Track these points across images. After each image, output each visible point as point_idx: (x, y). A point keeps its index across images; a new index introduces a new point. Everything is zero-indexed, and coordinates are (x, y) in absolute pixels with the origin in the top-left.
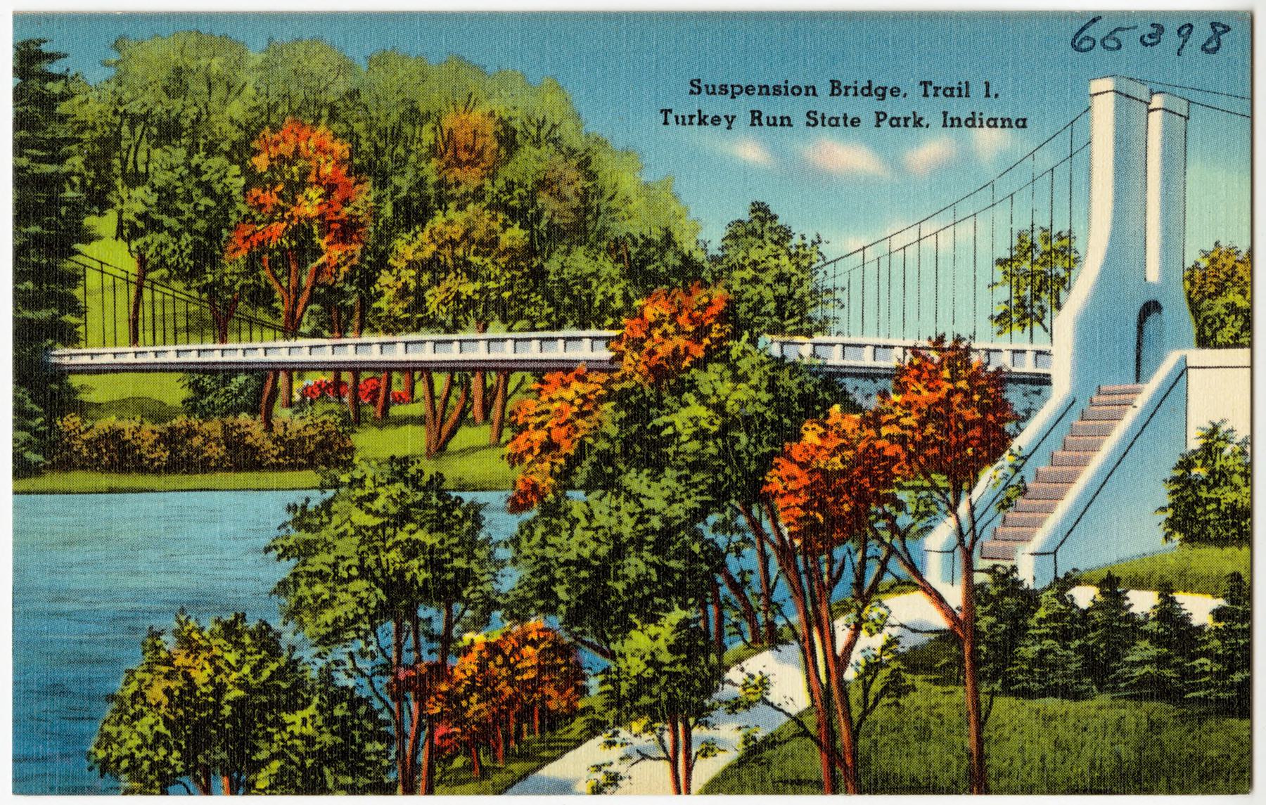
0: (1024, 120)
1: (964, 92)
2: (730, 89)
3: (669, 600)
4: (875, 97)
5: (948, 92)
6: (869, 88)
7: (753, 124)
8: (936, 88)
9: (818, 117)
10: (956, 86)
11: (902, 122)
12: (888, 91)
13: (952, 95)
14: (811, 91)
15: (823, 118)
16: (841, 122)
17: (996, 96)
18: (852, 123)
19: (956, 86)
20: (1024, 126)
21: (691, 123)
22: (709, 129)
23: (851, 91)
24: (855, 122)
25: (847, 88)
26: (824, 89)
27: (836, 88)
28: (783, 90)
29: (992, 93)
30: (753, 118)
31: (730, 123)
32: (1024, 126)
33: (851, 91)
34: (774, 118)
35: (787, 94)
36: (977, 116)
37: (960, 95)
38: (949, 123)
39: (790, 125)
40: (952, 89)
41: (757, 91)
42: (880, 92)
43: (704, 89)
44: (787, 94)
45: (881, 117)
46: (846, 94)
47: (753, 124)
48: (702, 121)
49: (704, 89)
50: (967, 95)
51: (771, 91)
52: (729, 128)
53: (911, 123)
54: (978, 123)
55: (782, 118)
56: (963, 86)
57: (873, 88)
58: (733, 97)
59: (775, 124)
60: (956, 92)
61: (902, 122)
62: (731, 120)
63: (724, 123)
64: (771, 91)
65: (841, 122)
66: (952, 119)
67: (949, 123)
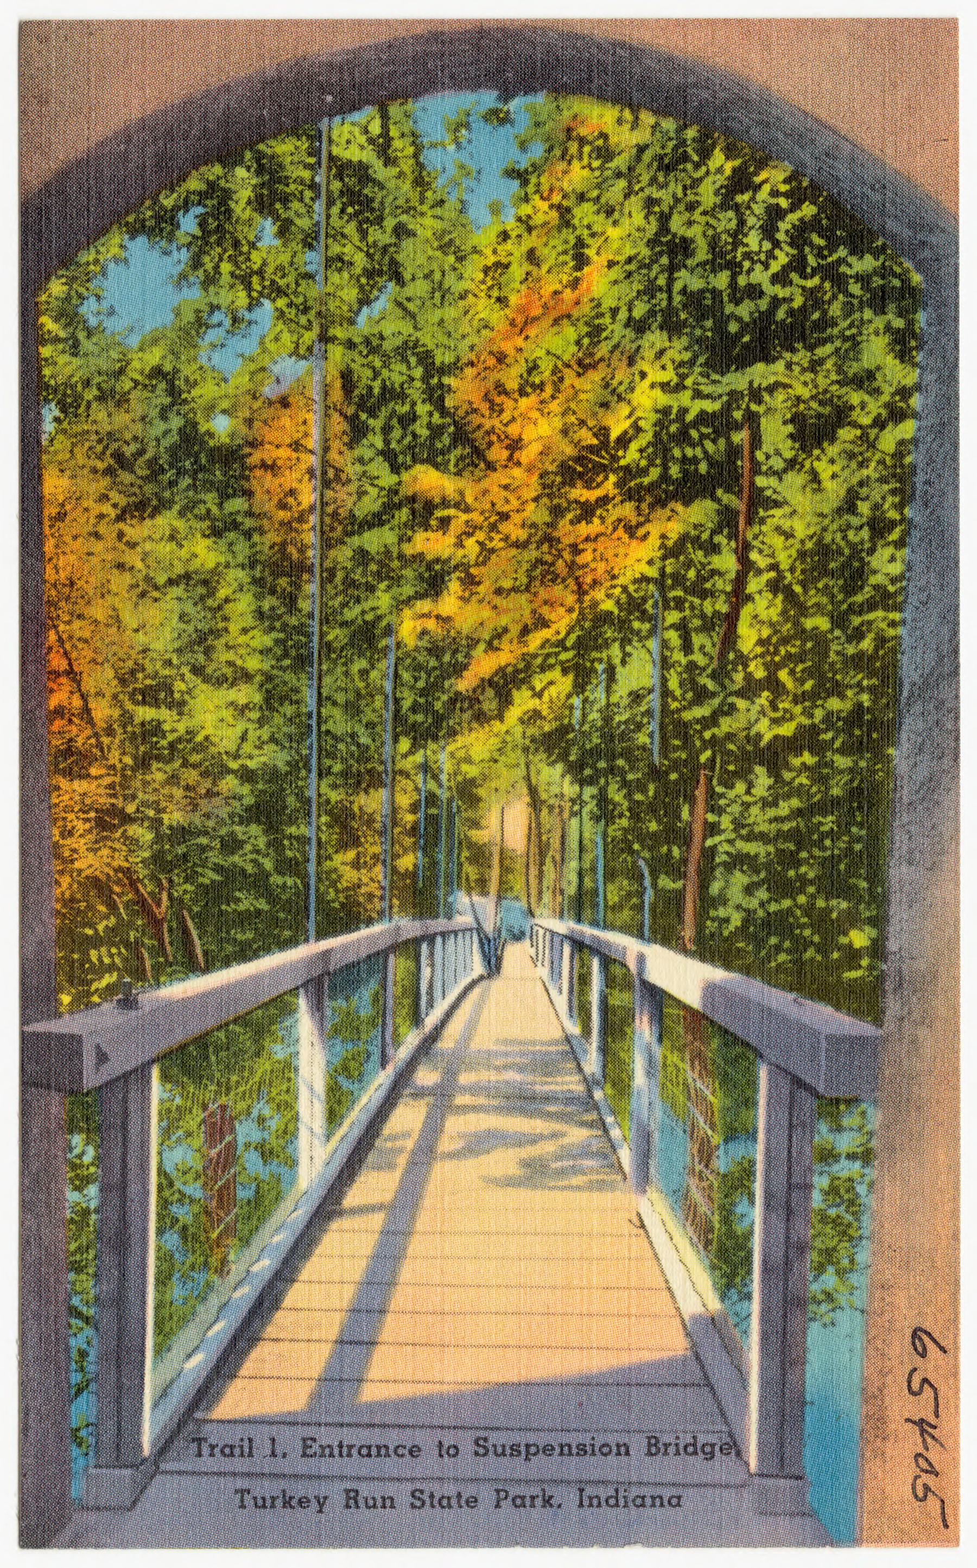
0: (679, 1498)
1: (246, 1450)
2: (523, 1449)
3: (385, 650)
4: (701, 1455)
5: (227, 1451)
6: (694, 1445)
7: (348, 1506)
8: (213, 1447)
9: (426, 1497)
10: (237, 1443)
11: (528, 1502)
12: (717, 1448)
13: (232, 1455)
14: (624, 1450)
15: (432, 1496)
16: (454, 1502)
17: (284, 1455)
18: (467, 1502)
19: (237, 1443)
20: (678, 1505)
21: (533, 1506)
22: (299, 1513)
23: (672, 1450)
24: (472, 1502)
25: (666, 1446)
26: (638, 1444)
27: (654, 1447)
28: (588, 1448)
29: (279, 1451)
30: (348, 1498)
31: (321, 1505)
32: (678, 1505)
33: (672, 1450)
34: (264, 1499)
35: (593, 1454)
36: (621, 1493)
37: (242, 1455)
38: (586, 1502)
39: (392, 1507)
40: (232, 1447)
41: (558, 1450)
42: (708, 1449)
43: (491, 1449)
44: (593, 1454)
45: (502, 1494)
46: (666, 1453)
47: (348, 1506)
48: (287, 1503)
49: (491, 1449)
50: (250, 1455)
51: (574, 1451)
52: (320, 1511)
53: (279, 1503)
54: (622, 1502)
55: (384, 1499)
56: (246, 1444)
57: (699, 1445)
58: (527, 1459)
59: (264, 1506)
60: (237, 1451)
61: (528, 1502)
62: (321, 1503)
63: (314, 1505)
64: (574, 1451)
65: (454, 1502)
66: (591, 1498)
67: (586, 1502)
